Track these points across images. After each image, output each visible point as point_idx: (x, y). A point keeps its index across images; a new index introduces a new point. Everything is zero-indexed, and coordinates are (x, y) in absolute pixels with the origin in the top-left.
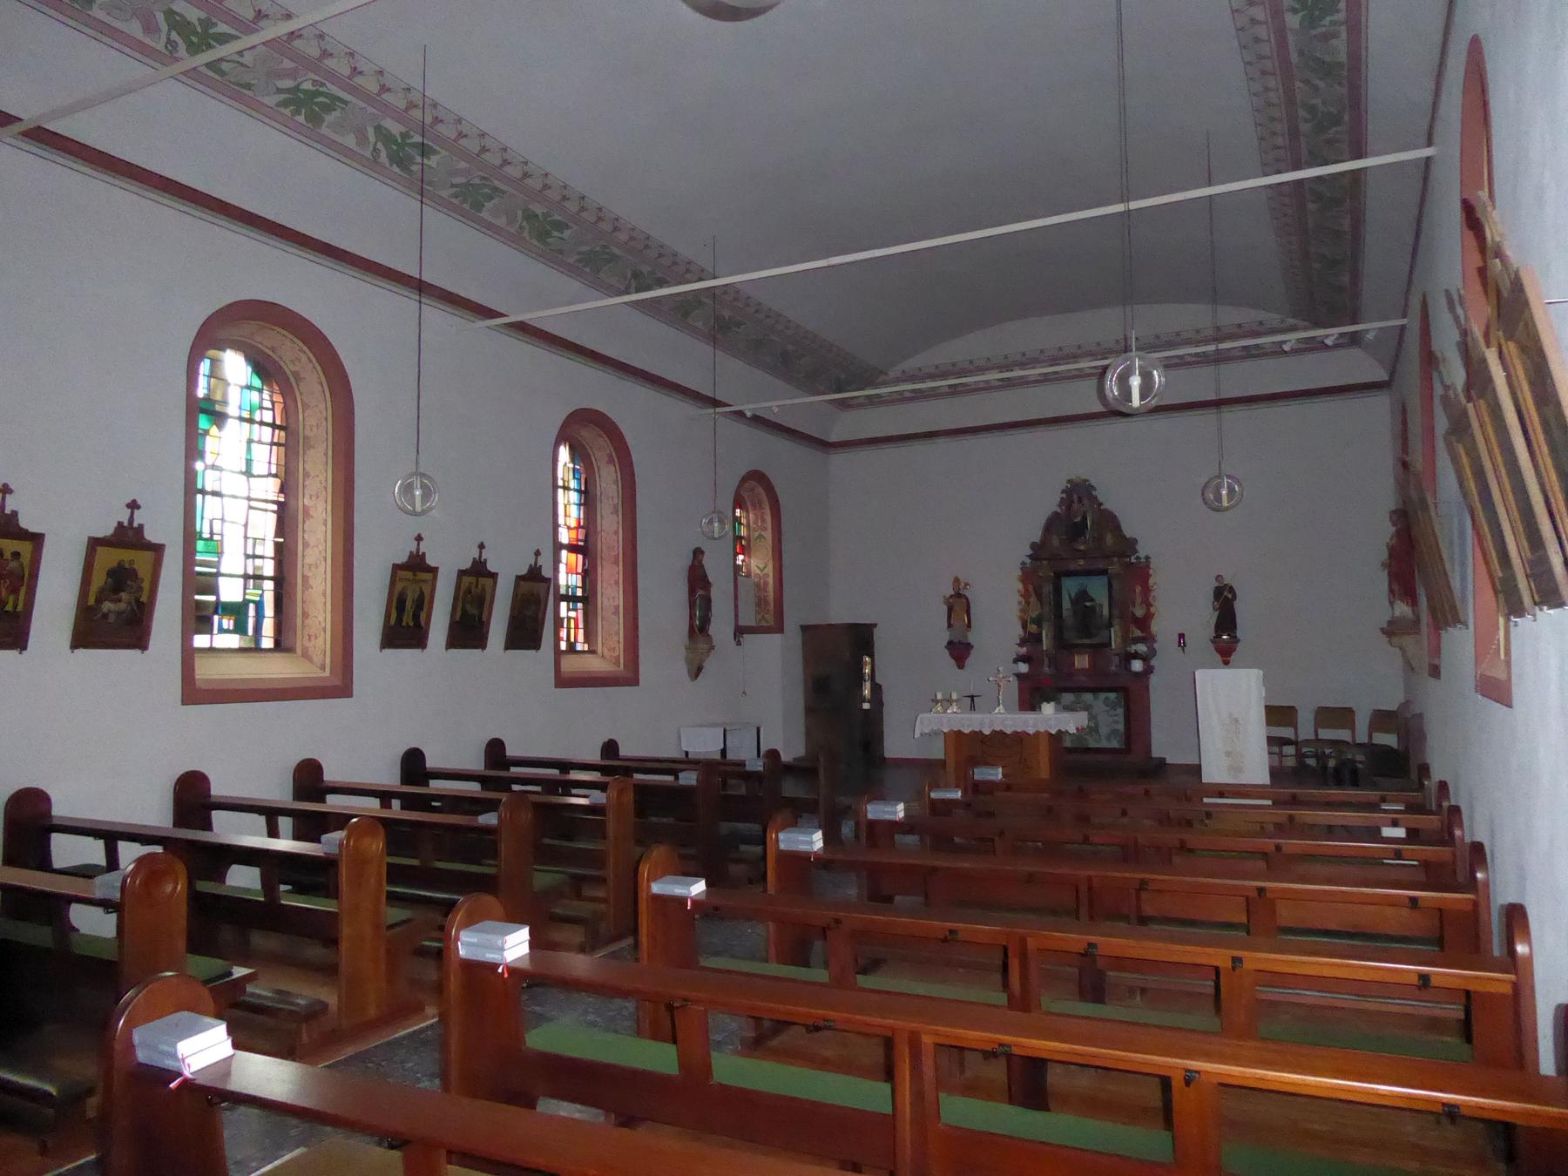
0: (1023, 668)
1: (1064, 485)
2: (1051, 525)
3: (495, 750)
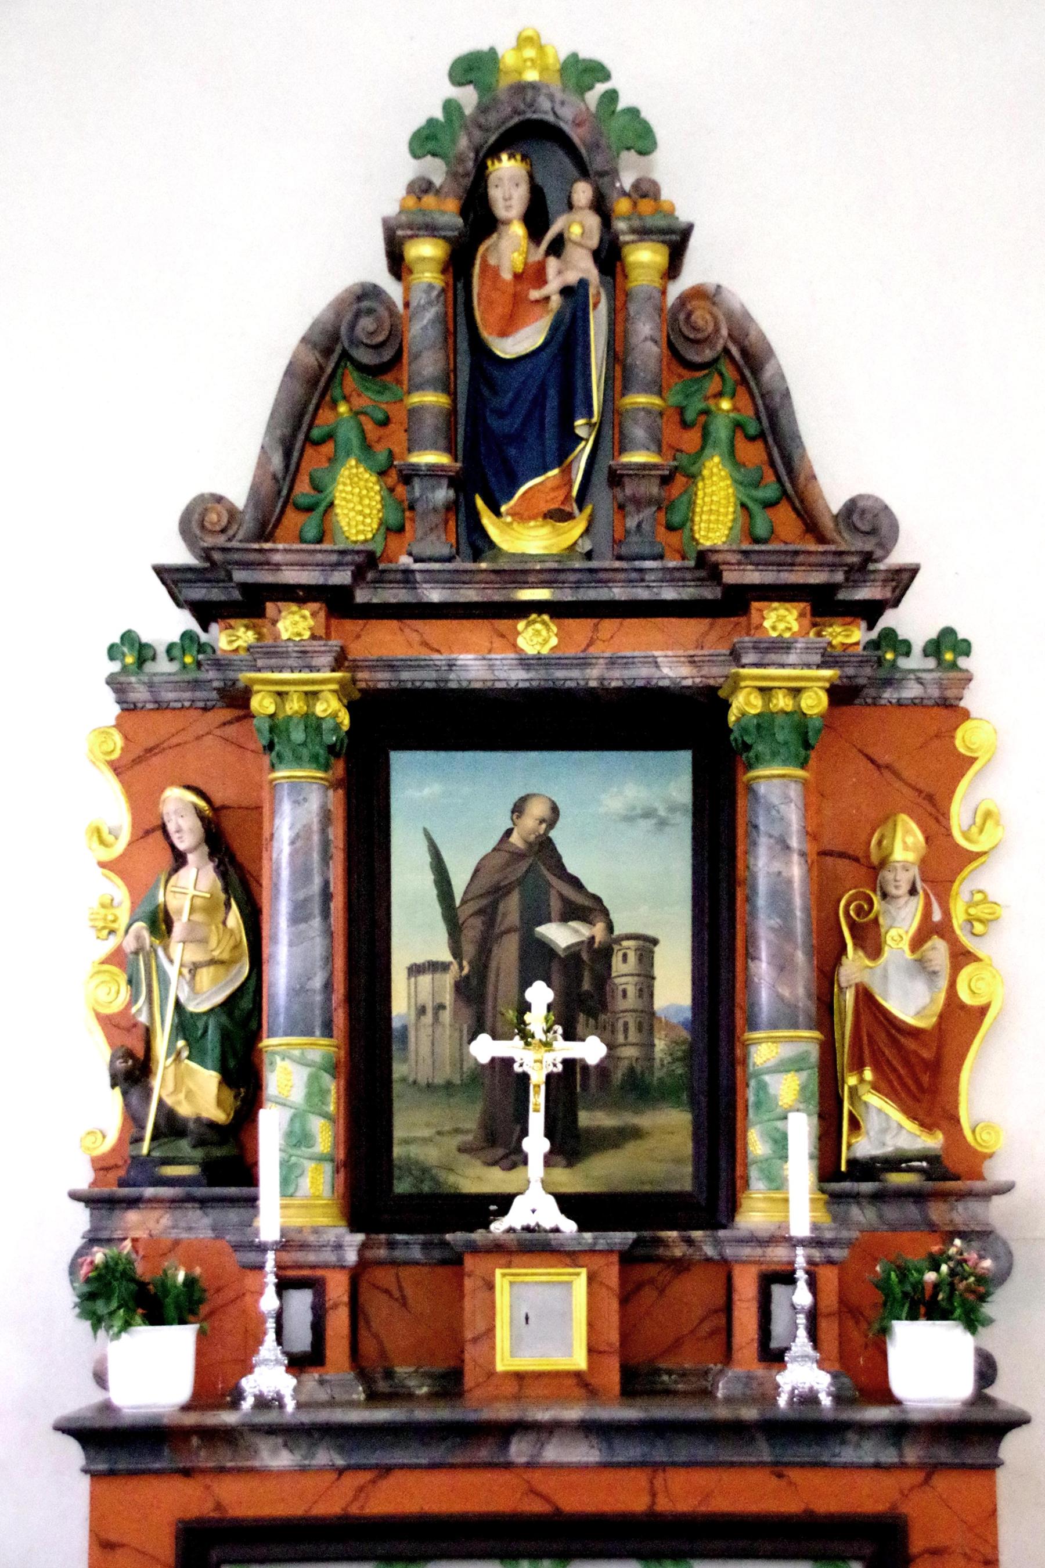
0: (154, 1370)
1: (431, 93)
2: (342, 366)
3: (1018, 1421)
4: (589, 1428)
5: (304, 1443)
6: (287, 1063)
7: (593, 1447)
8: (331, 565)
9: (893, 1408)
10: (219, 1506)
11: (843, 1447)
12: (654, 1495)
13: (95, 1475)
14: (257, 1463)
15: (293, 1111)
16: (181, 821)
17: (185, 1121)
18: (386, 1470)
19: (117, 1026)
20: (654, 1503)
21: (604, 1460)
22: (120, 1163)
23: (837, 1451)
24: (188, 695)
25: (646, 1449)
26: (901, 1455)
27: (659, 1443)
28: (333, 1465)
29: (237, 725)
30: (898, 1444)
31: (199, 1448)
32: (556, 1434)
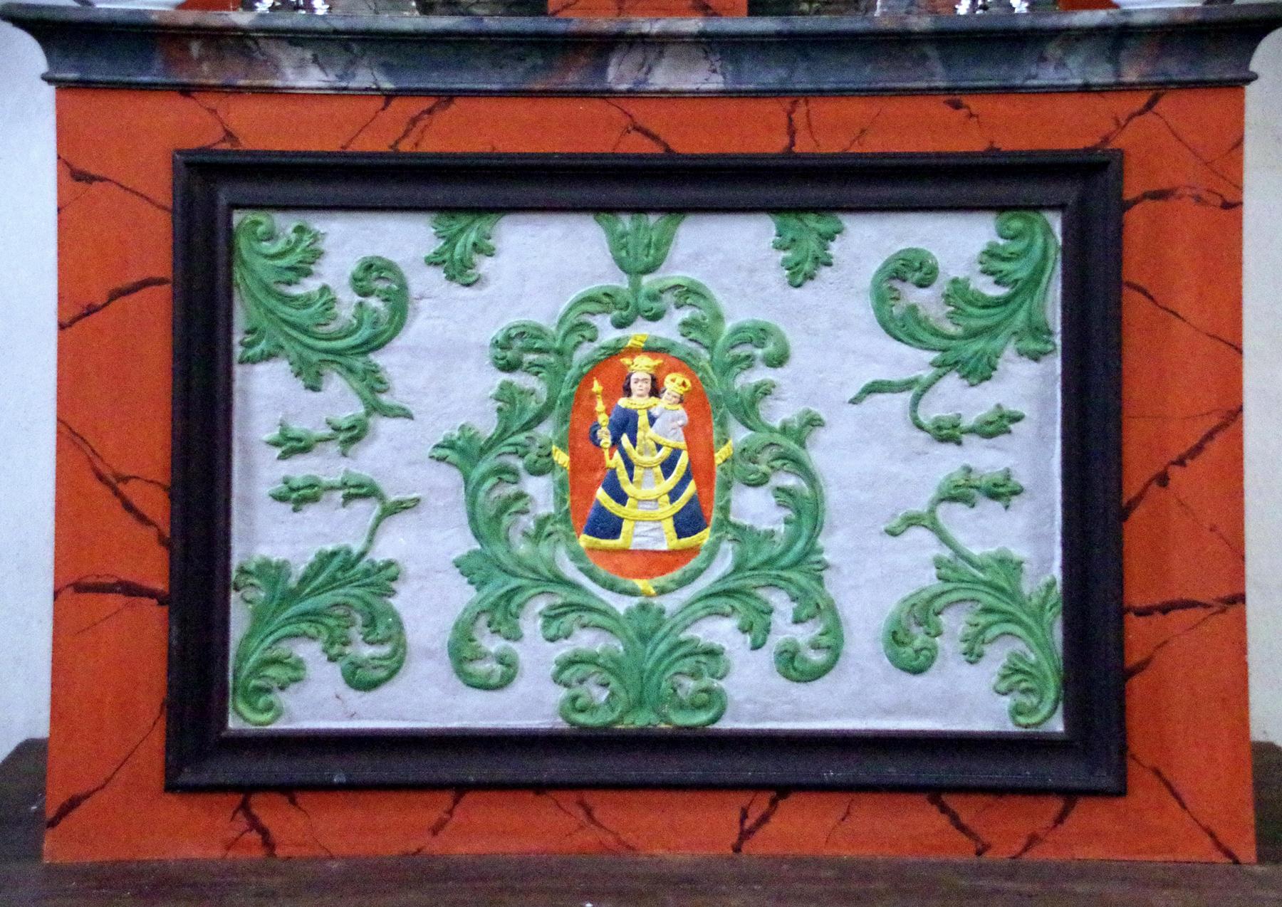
4: (708, 44)
5: (341, 59)
7: (714, 71)
8: (281, 663)
9: (1112, 11)
10: (229, 135)
11: (1042, 65)
12: (792, 133)
13: (62, 86)
14: (278, 83)
18: (449, 96)
20: (792, 144)
21: (729, 87)
23: (1033, 70)
25: (783, 73)
26: (1118, 73)
27: (803, 65)
28: (378, 89)
30: (1113, 59)
31: (200, 60)
32: (670, 50)
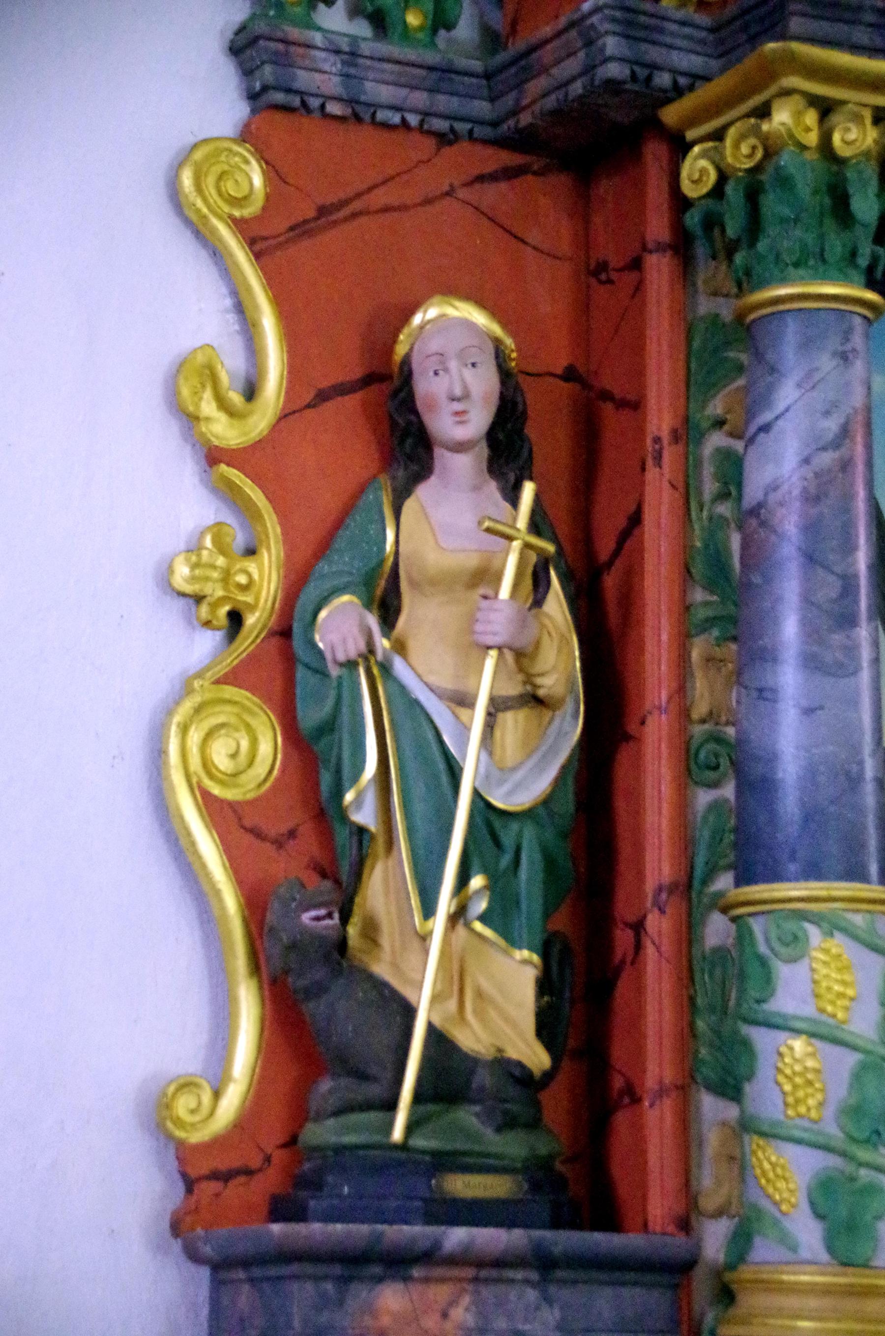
6: (838, 944)
15: (858, 1056)
16: (468, 374)
17: (471, 1062)
19: (257, 833)
22: (256, 1162)
24: (420, 99)
29: (503, 186)
